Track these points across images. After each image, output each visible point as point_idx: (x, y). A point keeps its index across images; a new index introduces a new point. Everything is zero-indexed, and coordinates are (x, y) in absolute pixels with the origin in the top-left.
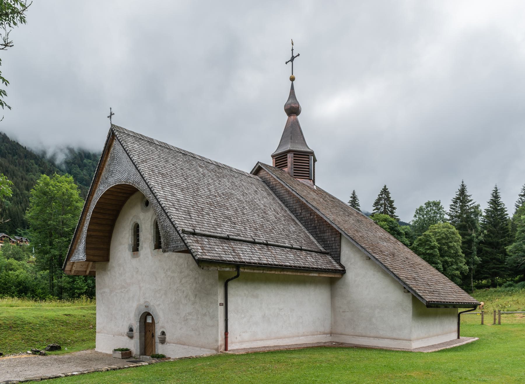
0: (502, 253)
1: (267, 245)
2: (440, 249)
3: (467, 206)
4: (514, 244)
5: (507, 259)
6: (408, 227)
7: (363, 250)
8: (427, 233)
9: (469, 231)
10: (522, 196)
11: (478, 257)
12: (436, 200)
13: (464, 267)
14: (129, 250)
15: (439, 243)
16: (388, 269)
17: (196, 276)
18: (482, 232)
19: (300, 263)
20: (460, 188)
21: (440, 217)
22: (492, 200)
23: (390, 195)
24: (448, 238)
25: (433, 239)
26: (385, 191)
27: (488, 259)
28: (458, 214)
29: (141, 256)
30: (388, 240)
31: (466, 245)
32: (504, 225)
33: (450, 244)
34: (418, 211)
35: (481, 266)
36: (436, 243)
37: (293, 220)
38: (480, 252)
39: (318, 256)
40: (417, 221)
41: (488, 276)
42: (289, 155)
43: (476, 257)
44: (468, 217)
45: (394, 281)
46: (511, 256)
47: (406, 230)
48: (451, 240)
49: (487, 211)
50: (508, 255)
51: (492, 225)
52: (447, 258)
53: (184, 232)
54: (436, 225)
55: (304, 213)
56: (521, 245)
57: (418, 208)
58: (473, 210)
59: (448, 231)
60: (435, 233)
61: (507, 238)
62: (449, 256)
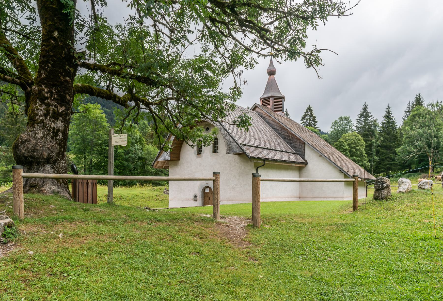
0: (394, 154)
1: (272, 150)
2: (350, 151)
3: (369, 120)
4: (402, 147)
5: (397, 157)
6: (326, 135)
7: (318, 152)
8: (341, 140)
9: (370, 138)
10: (407, 112)
11: (377, 156)
12: (346, 115)
13: (367, 163)
14: (195, 154)
15: (349, 147)
16: (331, 161)
17: (240, 166)
18: (379, 138)
19: (287, 159)
20: (363, 107)
21: (349, 128)
22: (386, 115)
23: (313, 113)
24: (355, 143)
25: (345, 144)
26: (309, 109)
27: (384, 158)
28: (362, 126)
29: (203, 157)
30: (328, 146)
31: (368, 148)
32: (395, 133)
33: (357, 147)
34: (334, 124)
35: (379, 163)
36: (347, 147)
37: (277, 136)
38: (378, 153)
39: (294, 155)
40: (333, 131)
41: (384, 170)
42: (271, 99)
43: (375, 157)
44: (369, 128)
45: (334, 167)
46: (400, 155)
47: (325, 138)
48: (357, 144)
49: (383, 123)
50: (398, 155)
51: (386, 133)
52: (355, 157)
53: (241, 144)
54: (347, 134)
55: (283, 132)
56: (406, 147)
57: (334, 121)
58: (372, 123)
59: (355, 138)
60: (347, 140)
61: (397, 142)
62: (357, 156)
